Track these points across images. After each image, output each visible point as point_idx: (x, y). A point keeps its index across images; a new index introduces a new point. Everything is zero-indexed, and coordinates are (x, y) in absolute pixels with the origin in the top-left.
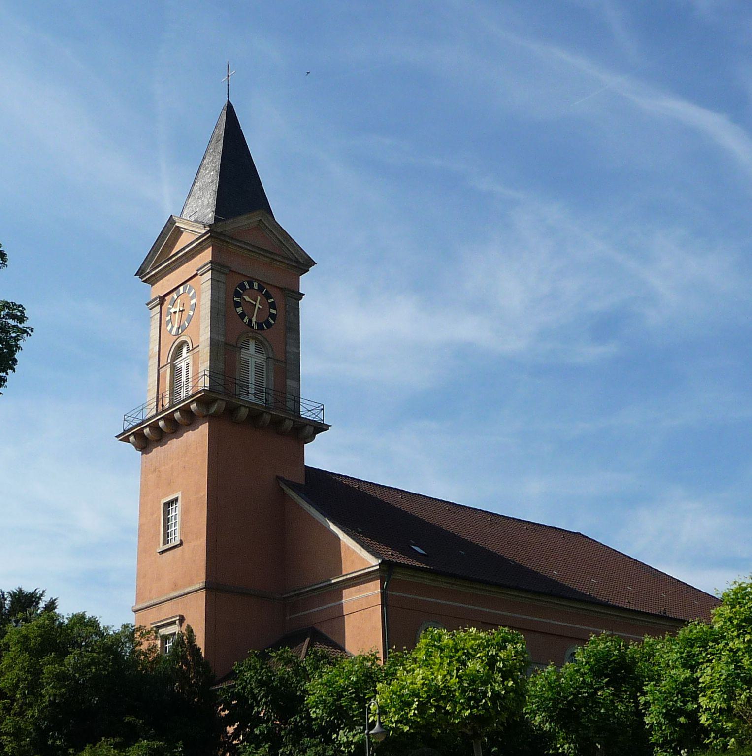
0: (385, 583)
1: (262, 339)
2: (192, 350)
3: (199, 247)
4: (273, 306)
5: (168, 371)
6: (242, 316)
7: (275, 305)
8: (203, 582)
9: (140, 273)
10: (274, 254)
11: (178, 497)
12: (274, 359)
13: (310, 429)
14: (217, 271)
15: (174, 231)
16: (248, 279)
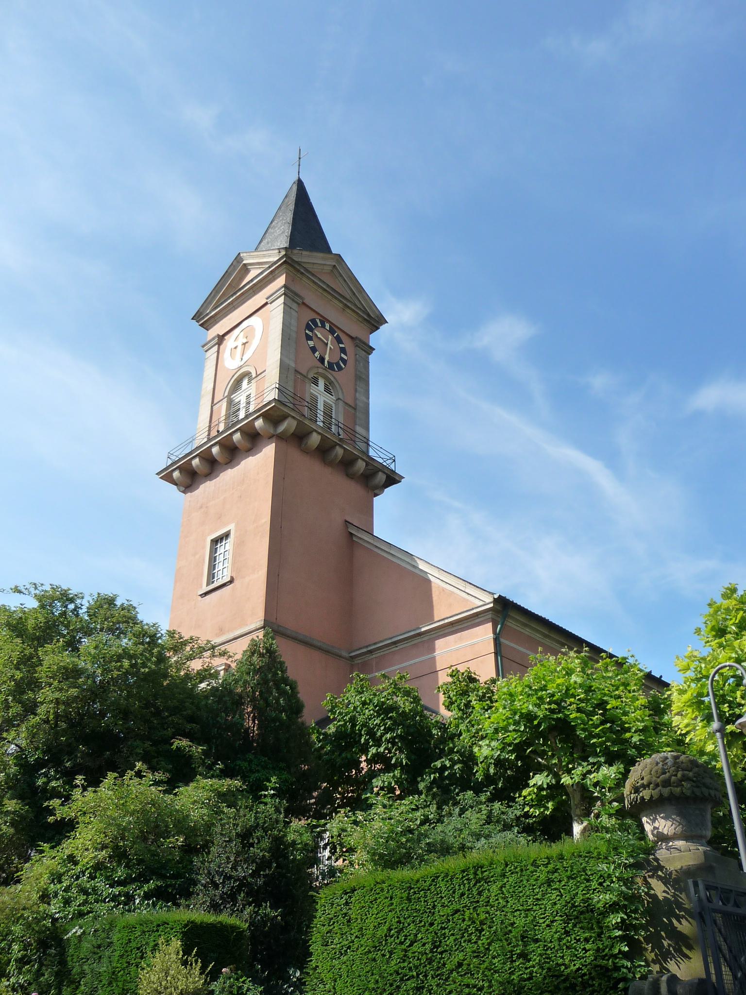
0: (499, 626)
1: (332, 379)
3: (271, 276)
4: (343, 351)
5: (223, 406)
6: (314, 349)
7: (345, 350)
8: (262, 620)
9: (197, 317)
10: (349, 301)
12: (344, 402)
13: (381, 477)
14: (290, 298)
15: (240, 271)
16: (321, 318)
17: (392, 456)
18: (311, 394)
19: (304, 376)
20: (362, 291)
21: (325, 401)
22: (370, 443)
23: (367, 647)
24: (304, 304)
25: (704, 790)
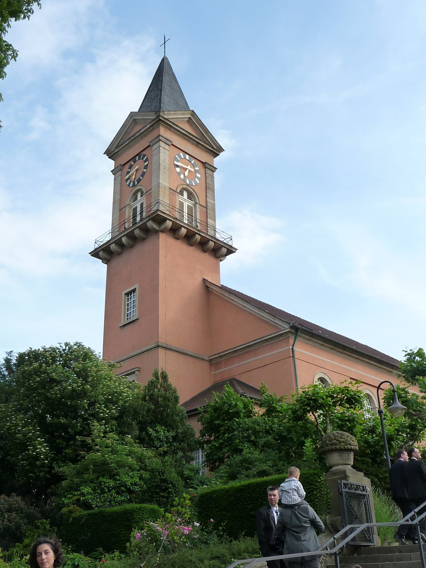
2: (146, 193)
11: (136, 288)
12: (200, 204)
13: (224, 250)
17: (229, 236)
18: (180, 201)
19: (175, 191)
20: (208, 132)
21: (188, 205)
22: (217, 230)
23: (219, 354)
24: (172, 145)
25: (349, 446)
